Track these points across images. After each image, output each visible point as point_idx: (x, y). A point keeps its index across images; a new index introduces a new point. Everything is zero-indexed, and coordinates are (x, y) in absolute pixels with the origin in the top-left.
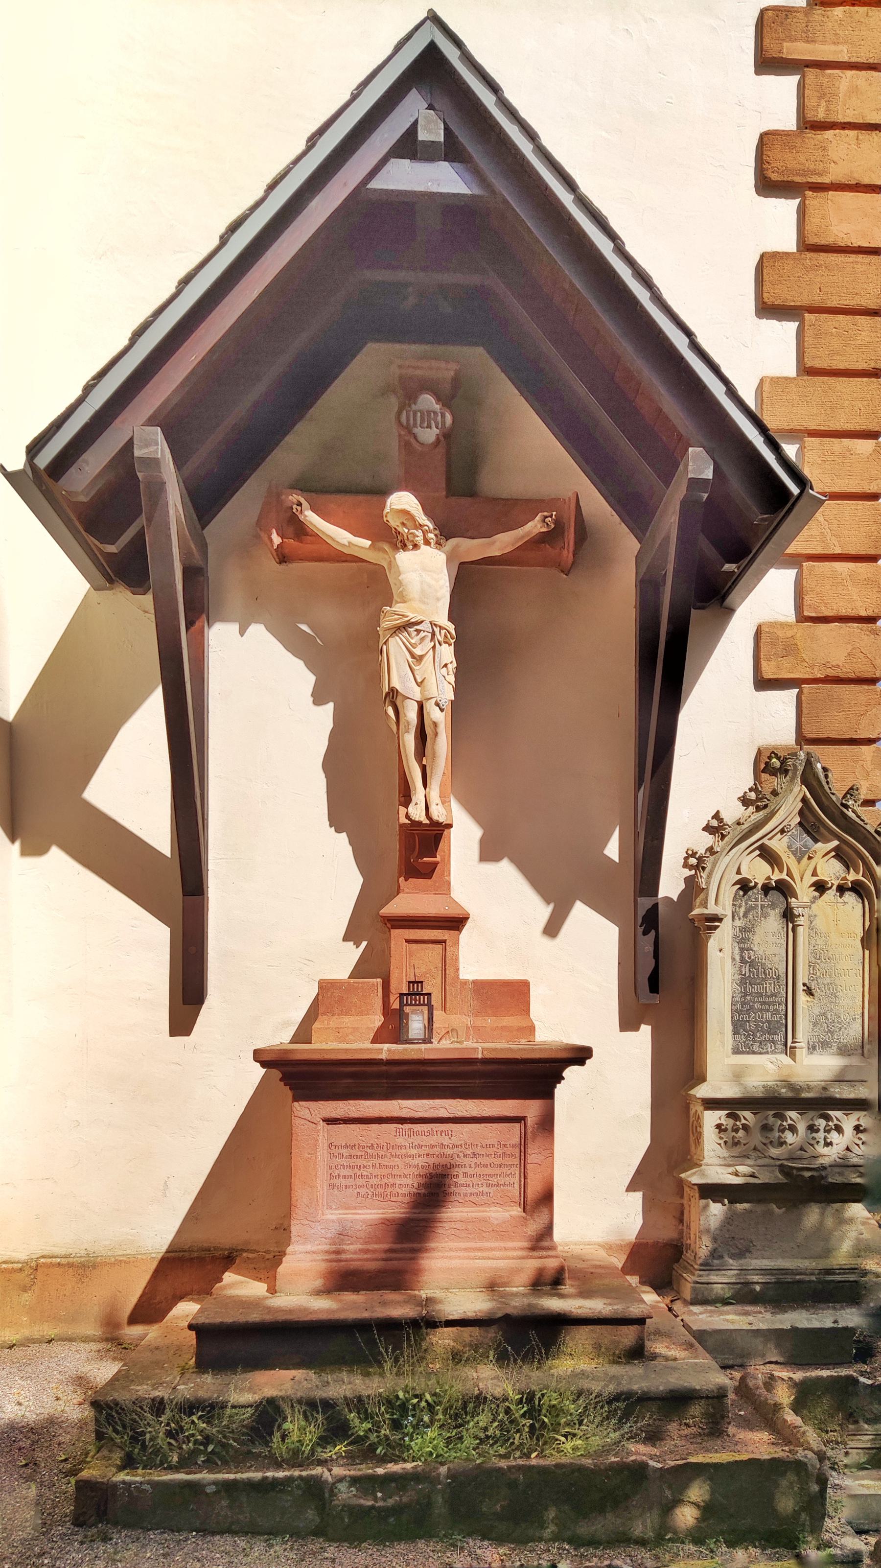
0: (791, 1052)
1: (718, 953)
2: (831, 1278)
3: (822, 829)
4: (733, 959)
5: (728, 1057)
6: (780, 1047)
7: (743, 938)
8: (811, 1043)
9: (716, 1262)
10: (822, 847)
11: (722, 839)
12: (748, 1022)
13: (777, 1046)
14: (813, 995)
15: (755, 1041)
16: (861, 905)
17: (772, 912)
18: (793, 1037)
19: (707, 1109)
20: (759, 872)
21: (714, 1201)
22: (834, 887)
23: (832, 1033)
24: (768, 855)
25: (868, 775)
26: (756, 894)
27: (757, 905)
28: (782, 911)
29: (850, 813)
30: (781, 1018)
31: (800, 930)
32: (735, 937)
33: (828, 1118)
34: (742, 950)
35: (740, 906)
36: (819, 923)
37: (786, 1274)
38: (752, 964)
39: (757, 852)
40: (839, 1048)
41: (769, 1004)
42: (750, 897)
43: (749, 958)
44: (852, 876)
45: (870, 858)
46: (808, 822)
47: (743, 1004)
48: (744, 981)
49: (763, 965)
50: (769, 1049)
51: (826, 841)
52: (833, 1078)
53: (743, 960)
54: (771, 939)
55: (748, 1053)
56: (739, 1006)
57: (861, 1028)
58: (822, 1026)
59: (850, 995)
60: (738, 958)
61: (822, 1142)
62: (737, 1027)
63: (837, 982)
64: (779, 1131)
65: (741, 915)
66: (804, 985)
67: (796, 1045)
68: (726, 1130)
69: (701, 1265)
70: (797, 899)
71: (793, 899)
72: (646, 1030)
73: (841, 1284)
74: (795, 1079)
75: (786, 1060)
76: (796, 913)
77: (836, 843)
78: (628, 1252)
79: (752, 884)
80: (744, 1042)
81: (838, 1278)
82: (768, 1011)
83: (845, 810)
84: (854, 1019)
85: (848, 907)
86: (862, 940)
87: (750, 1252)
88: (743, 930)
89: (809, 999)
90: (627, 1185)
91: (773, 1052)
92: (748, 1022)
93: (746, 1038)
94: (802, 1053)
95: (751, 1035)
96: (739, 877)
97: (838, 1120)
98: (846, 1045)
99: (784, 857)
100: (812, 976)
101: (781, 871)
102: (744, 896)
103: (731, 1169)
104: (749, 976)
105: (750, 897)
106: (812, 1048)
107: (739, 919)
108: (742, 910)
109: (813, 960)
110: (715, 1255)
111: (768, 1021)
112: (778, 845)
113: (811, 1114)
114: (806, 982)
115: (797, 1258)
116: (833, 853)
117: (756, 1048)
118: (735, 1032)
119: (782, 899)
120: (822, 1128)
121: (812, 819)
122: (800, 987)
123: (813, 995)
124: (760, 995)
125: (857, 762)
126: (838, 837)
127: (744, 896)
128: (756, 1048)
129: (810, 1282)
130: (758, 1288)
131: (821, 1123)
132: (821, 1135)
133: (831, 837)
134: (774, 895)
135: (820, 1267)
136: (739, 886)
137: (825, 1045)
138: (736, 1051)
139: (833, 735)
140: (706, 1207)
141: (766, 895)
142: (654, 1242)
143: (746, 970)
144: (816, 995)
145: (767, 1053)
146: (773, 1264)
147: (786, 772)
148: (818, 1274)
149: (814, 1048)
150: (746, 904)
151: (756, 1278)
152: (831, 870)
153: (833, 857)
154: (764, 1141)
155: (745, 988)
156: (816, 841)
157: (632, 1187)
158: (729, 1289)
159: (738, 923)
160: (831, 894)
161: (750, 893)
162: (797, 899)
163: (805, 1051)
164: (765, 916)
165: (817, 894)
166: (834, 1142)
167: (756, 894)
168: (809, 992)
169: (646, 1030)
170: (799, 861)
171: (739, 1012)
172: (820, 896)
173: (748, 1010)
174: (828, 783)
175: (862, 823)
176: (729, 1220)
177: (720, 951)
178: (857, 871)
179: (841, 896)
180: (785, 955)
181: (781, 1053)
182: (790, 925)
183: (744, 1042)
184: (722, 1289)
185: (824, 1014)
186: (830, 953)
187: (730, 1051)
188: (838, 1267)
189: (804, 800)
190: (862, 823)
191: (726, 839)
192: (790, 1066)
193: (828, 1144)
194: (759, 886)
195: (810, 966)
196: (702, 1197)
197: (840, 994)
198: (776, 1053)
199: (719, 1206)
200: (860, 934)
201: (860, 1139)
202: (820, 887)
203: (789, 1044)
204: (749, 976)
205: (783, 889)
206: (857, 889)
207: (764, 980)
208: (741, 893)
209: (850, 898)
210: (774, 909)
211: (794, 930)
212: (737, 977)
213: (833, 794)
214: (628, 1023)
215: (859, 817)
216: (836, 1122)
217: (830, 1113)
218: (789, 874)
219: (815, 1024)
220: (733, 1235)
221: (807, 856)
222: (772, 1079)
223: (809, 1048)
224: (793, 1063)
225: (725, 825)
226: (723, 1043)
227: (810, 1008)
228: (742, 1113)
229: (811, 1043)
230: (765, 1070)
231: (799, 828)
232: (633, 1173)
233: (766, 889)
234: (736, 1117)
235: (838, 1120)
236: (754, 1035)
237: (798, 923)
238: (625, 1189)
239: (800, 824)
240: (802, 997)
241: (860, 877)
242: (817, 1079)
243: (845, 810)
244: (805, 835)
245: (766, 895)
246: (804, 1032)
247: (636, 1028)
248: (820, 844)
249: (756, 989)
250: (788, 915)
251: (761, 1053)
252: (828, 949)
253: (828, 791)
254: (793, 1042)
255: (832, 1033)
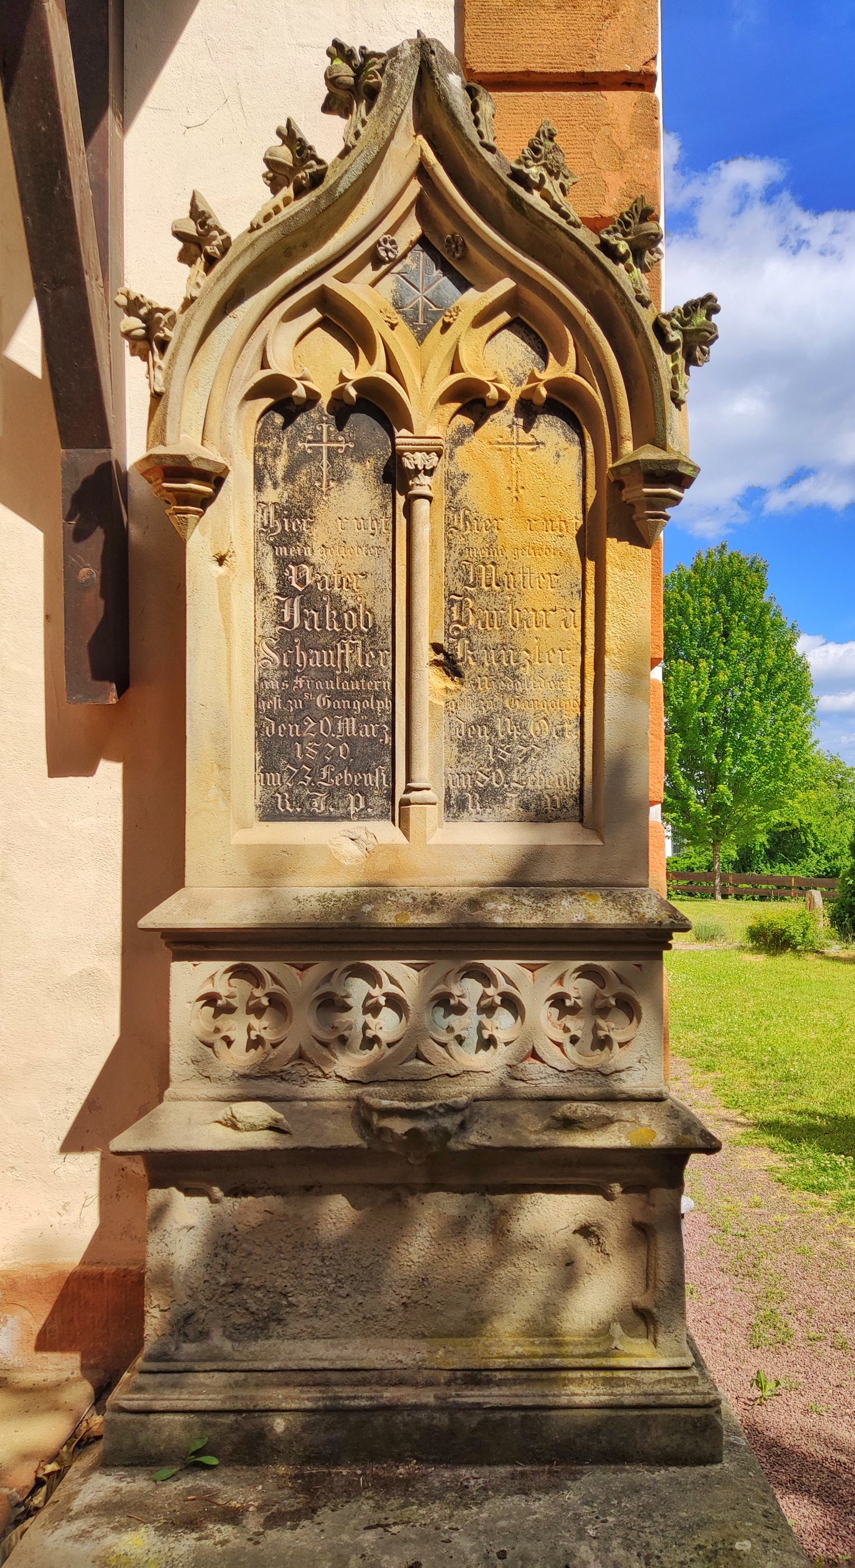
0: (398, 812)
1: (215, 566)
2: (473, 1396)
3: (474, 252)
4: (260, 585)
5: (245, 826)
6: (378, 801)
7: (285, 533)
8: (455, 793)
9: (189, 1348)
10: (475, 300)
11: (208, 268)
12: (300, 740)
13: (373, 801)
14: (459, 674)
15: (318, 789)
16: (576, 449)
17: (356, 469)
18: (408, 779)
19: (179, 956)
20: (324, 366)
21: (188, 1192)
22: (511, 405)
23: (506, 767)
24: (345, 325)
25: (622, 159)
26: (317, 422)
27: (318, 451)
28: (381, 464)
29: (534, 199)
30: (380, 730)
31: (422, 508)
32: (265, 529)
33: (486, 977)
34: (282, 563)
35: (276, 454)
36: (473, 494)
37: (364, 1383)
38: (309, 597)
39: (314, 315)
40: (525, 806)
41: (351, 696)
42: (300, 430)
43: (302, 581)
44: (553, 371)
45: (590, 318)
46: (441, 237)
47: (287, 696)
48: (287, 639)
49: (336, 600)
50: (352, 809)
51: (486, 283)
52: (502, 877)
53: (285, 589)
54: (354, 536)
55: (300, 818)
56: (276, 702)
57: (577, 755)
58: (480, 751)
59: (550, 673)
60: (271, 582)
61: (472, 1039)
62: (272, 752)
63: (519, 640)
64: (366, 1010)
65: (280, 474)
66: (437, 648)
67: (413, 796)
68: (229, 1010)
69: (149, 1358)
70: (411, 429)
71: (404, 432)
72: (110, 774)
73: (498, 1415)
74: (409, 881)
75: (386, 832)
76: (408, 464)
77: (506, 285)
78: (55, 1296)
79: (300, 392)
80: (290, 791)
81: (494, 1396)
82: (349, 713)
83: (520, 190)
84: (561, 733)
85: (545, 454)
86: (581, 536)
87: (279, 1321)
88: (285, 512)
89: (452, 686)
90: (63, 1134)
91: (362, 816)
92: (300, 740)
93: (295, 779)
94: (428, 819)
95: (306, 774)
96: (266, 373)
97: (509, 981)
98: (539, 798)
99: (379, 327)
100: (456, 628)
101: (371, 359)
102: (285, 426)
103: (224, 1111)
104: (302, 627)
105: (300, 430)
106: (455, 806)
107: (275, 485)
108: (281, 464)
109: (460, 587)
110: (190, 1331)
111: (349, 740)
112: (366, 295)
113: (442, 966)
114: (441, 640)
115: (401, 1335)
116: (504, 317)
117: (319, 804)
118: (267, 766)
119: (381, 434)
120: (471, 1002)
121: (448, 227)
122: (424, 654)
123: (459, 674)
124: (329, 674)
125: (596, 128)
126: (513, 271)
127: (285, 426)
128: (319, 804)
129: (416, 1408)
130: (279, 1424)
131: (470, 991)
132: (467, 1023)
133: (493, 269)
134: (362, 424)
135: (456, 1362)
136: (267, 402)
137: (488, 796)
138: (270, 813)
139: (536, 66)
140: (161, 1210)
141: (340, 426)
142: (117, 1273)
143: (293, 611)
144: (467, 673)
145: (347, 817)
146: (332, 1353)
147: (371, 94)
148: (448, 1384)
149: (462, 805)
150: (292, 446)
151: (277, 1396)
152: (503, 361)
153: (507, 326)
154: (324, 1037)
155: (291, 659)
156: (463, 285)
157: (75, 1142)
158: (206, 1425)
159: (271, 495)
160: (502, 421)
161: (301, 420)
162: (411, 429)
163: (434, 813)
164: (339, 477)
165: (464, 421)
166: (501, 1036)
167: (317, 422)
168: (450, 666)
169: (110, 774)
170: (421, 338)
171: (277, 717)
172: (477, 427)
173: (298, 712)
174: (477, 122)
175: (563, 222)
176: (222, 1242)
177: (221, 560)
178: (562, 360)
179: (527, 428)
180: (389, 575)
181: (382, 816)
182: (401, 500)
183: (290, 791)
184: (187, 1427)
185: (485, 721)
186: (502, 569)
187: (251, 811)
188: (499, 1363)
189: (422, 172)
190: (563, 222)
191: (219, 267)
192: (394, 849)
193: (488, 1043)
194: (325, 400)
195: (451, 602)
196: (157, 1182)
197: (526, 672)
198: (368, 817)
199: (202, 1202)
200: (575, 519)
201: (566, 1030)
202: (472, 401)
203: (399, 795)
204: (302, 627)
205: (376, 405)
206: (561, 404)
207: (340, 637)
208: (279, 419)
209: (550, 430)
210: (361, 460)
211: (408, 511)
212: (270, 629)
213: (492, 149)
214: (68, 757)
215: (556, 207)
216: (503, 986)
217: (489, 963)
218: (392, 368)
219: (464, 746)
220: (237, 1277)
221: (439, 324)
222: (351, 879)
223: (448, 806)
224: (404, 840)
225: (211, 229)
226: (226, 793)
227: (451, 708)
228: (382, 966)
229: (455, 793)
230: (334, 857)
231: (423, 255)
232: (79, 1107)
233: (342, 409)
234: (256, 979)
235: (509, 981)
236: (315, 774)
237: (417, 490)
238: (59, 1144)
239: (423, 242)
240: (431, 682)
241: (569, 371)
242: (460, 879)
243: (520, 190)
244: (437, 273)
245: (340, 426)
246: (432, 763)
247: (87, 769)
248: (472, 291)
249: (318, 659)
250: (395, 476)
251: (330, 818)
252: (497, 558)
253: (476, 140)
254: (408, 790)
255: (506, 767)
